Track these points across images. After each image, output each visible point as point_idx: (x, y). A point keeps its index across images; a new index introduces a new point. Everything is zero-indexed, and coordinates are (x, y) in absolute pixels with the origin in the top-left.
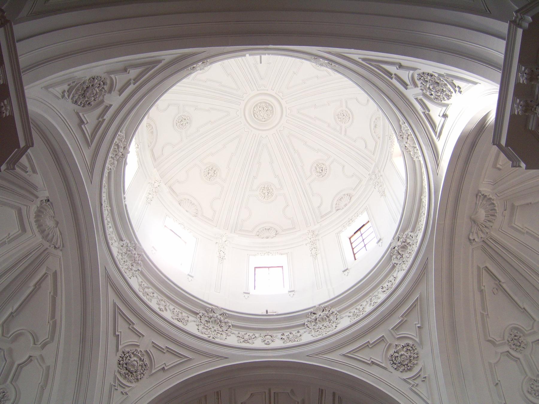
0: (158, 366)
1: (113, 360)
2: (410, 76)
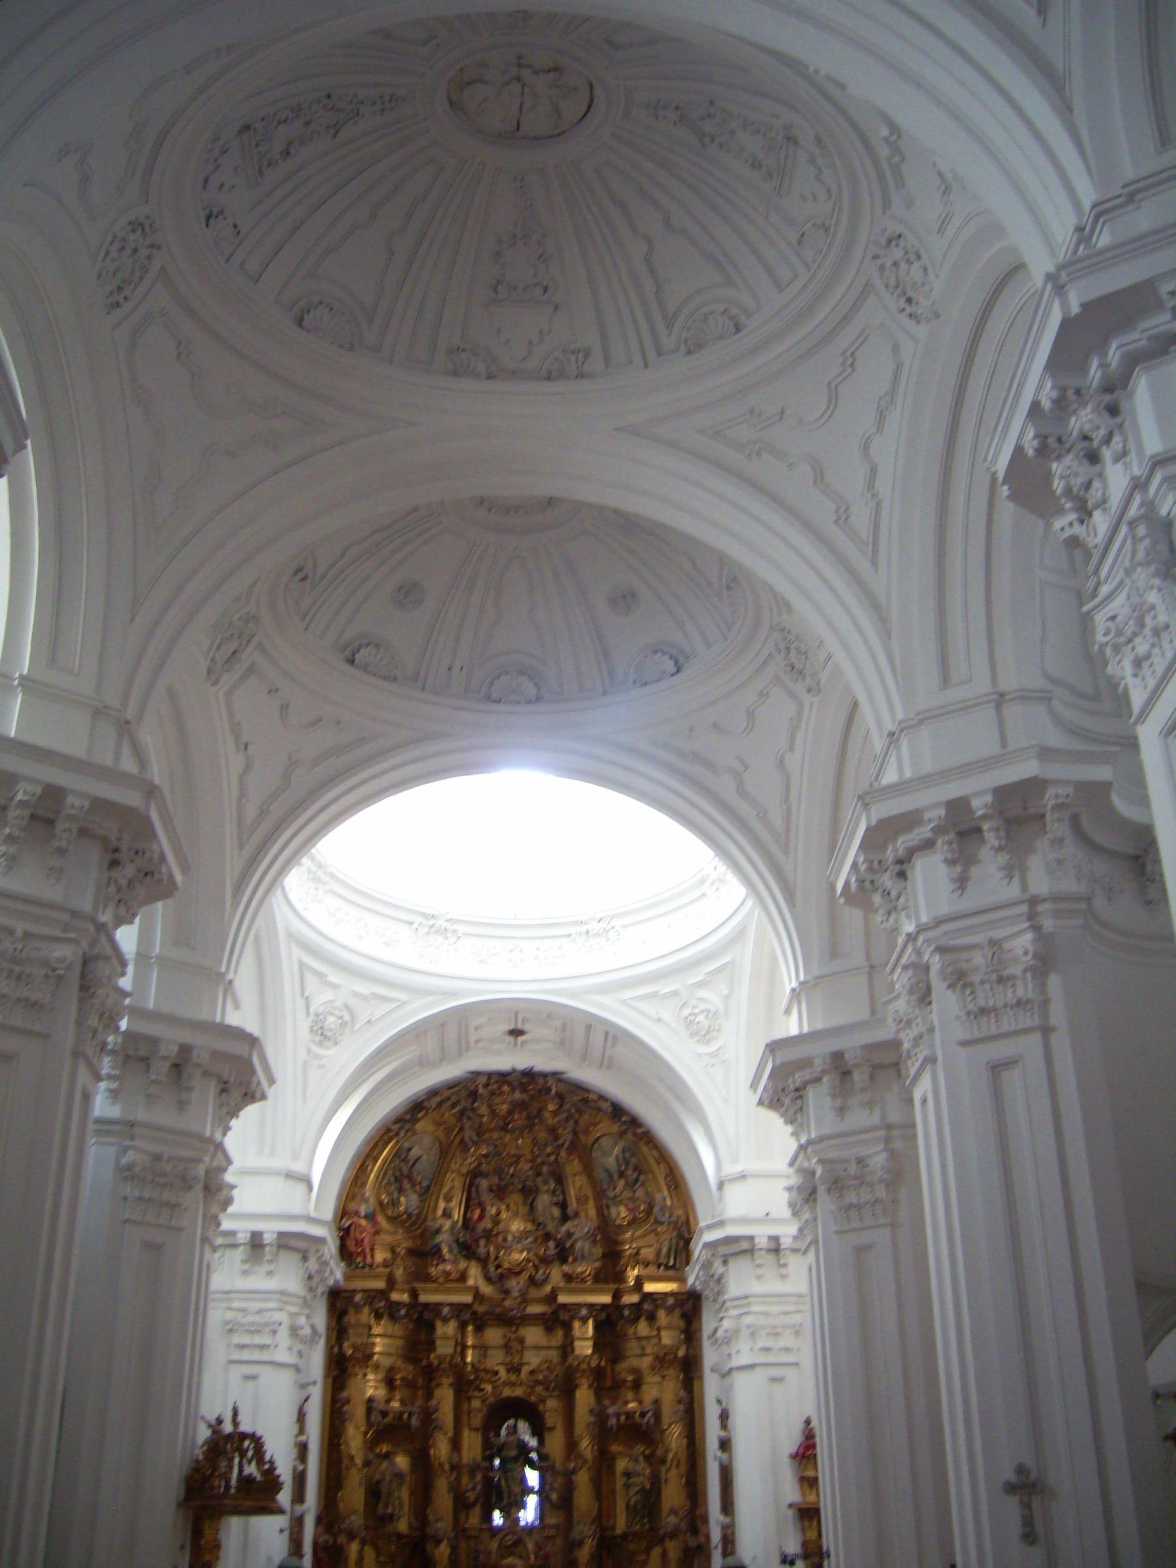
0: (362, 1019)
1: (304, 1025)
2: (779, 755)
